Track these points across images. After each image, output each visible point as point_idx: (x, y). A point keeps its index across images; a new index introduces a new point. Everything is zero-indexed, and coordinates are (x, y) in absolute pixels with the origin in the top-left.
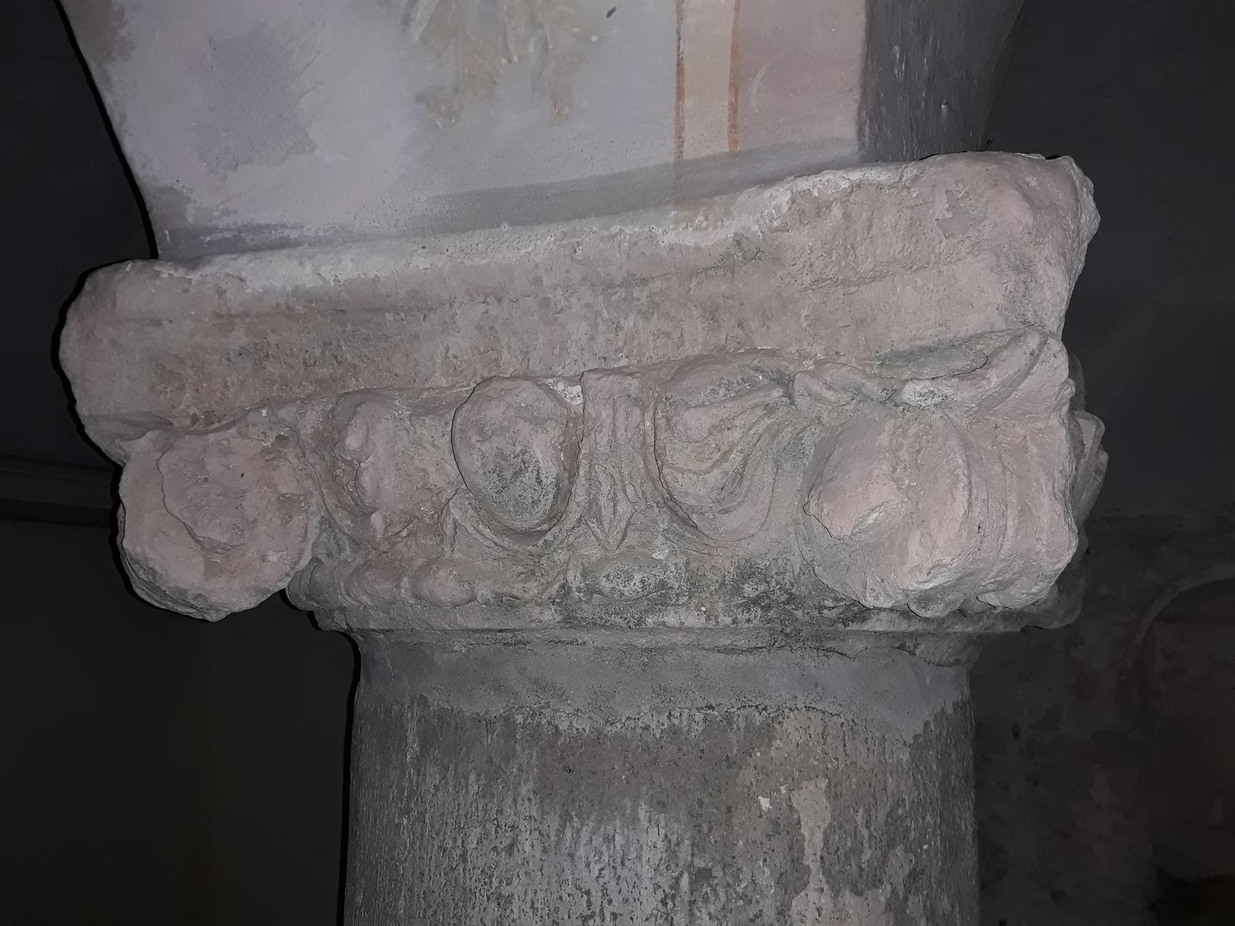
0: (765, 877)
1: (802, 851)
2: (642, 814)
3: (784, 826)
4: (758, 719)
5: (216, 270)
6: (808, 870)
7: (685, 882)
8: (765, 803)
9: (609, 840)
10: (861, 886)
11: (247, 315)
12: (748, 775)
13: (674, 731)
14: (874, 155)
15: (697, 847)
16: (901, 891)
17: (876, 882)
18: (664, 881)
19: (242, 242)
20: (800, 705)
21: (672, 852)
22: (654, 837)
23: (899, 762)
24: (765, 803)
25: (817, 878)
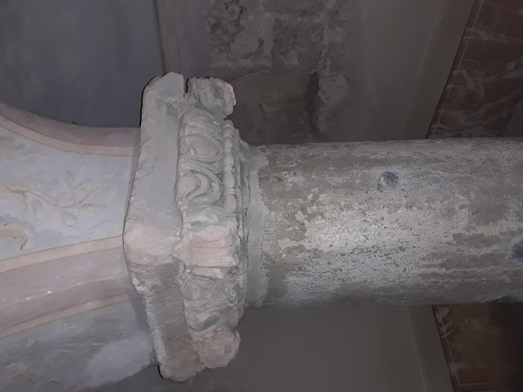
0: (300, 256)
1: (295, 246)
2: (286, 280)
3: (289, 251)
4: (264, 257)
5: (160, 358)
6: (300, 245)
7: (301, 272)
8: (284, 256)
9: (291, 286)
10: (304, 229)
11: (188, 288)
12: (277, 260)
13: (267, 275)
14: (138, 143)
15: (294, 270)
16: (306, 216)
17: (303, 224)
18: (300, 276)
19: (154, 354)
20: (261, 247)
21: (294, 275)
22: (291, 278)
23: (275, 215)
24: (284, 256)
25: (301, 242)
